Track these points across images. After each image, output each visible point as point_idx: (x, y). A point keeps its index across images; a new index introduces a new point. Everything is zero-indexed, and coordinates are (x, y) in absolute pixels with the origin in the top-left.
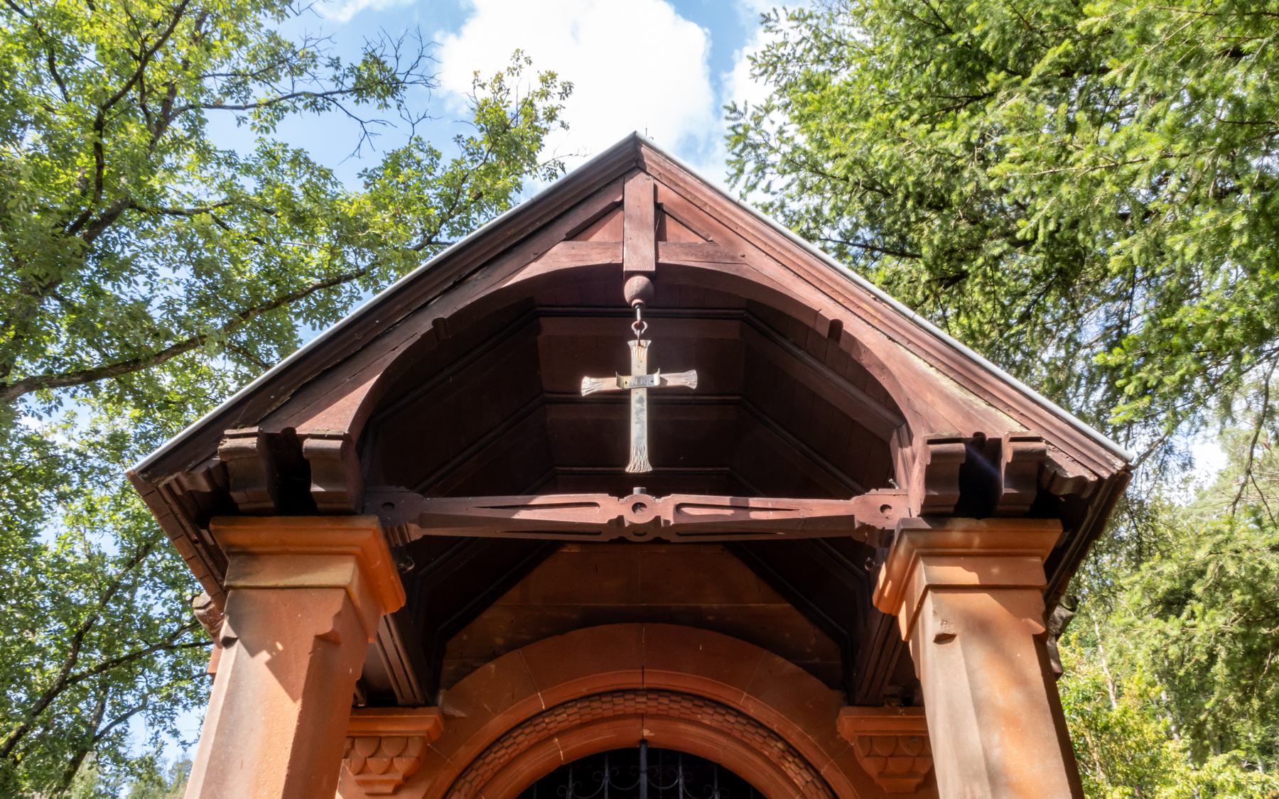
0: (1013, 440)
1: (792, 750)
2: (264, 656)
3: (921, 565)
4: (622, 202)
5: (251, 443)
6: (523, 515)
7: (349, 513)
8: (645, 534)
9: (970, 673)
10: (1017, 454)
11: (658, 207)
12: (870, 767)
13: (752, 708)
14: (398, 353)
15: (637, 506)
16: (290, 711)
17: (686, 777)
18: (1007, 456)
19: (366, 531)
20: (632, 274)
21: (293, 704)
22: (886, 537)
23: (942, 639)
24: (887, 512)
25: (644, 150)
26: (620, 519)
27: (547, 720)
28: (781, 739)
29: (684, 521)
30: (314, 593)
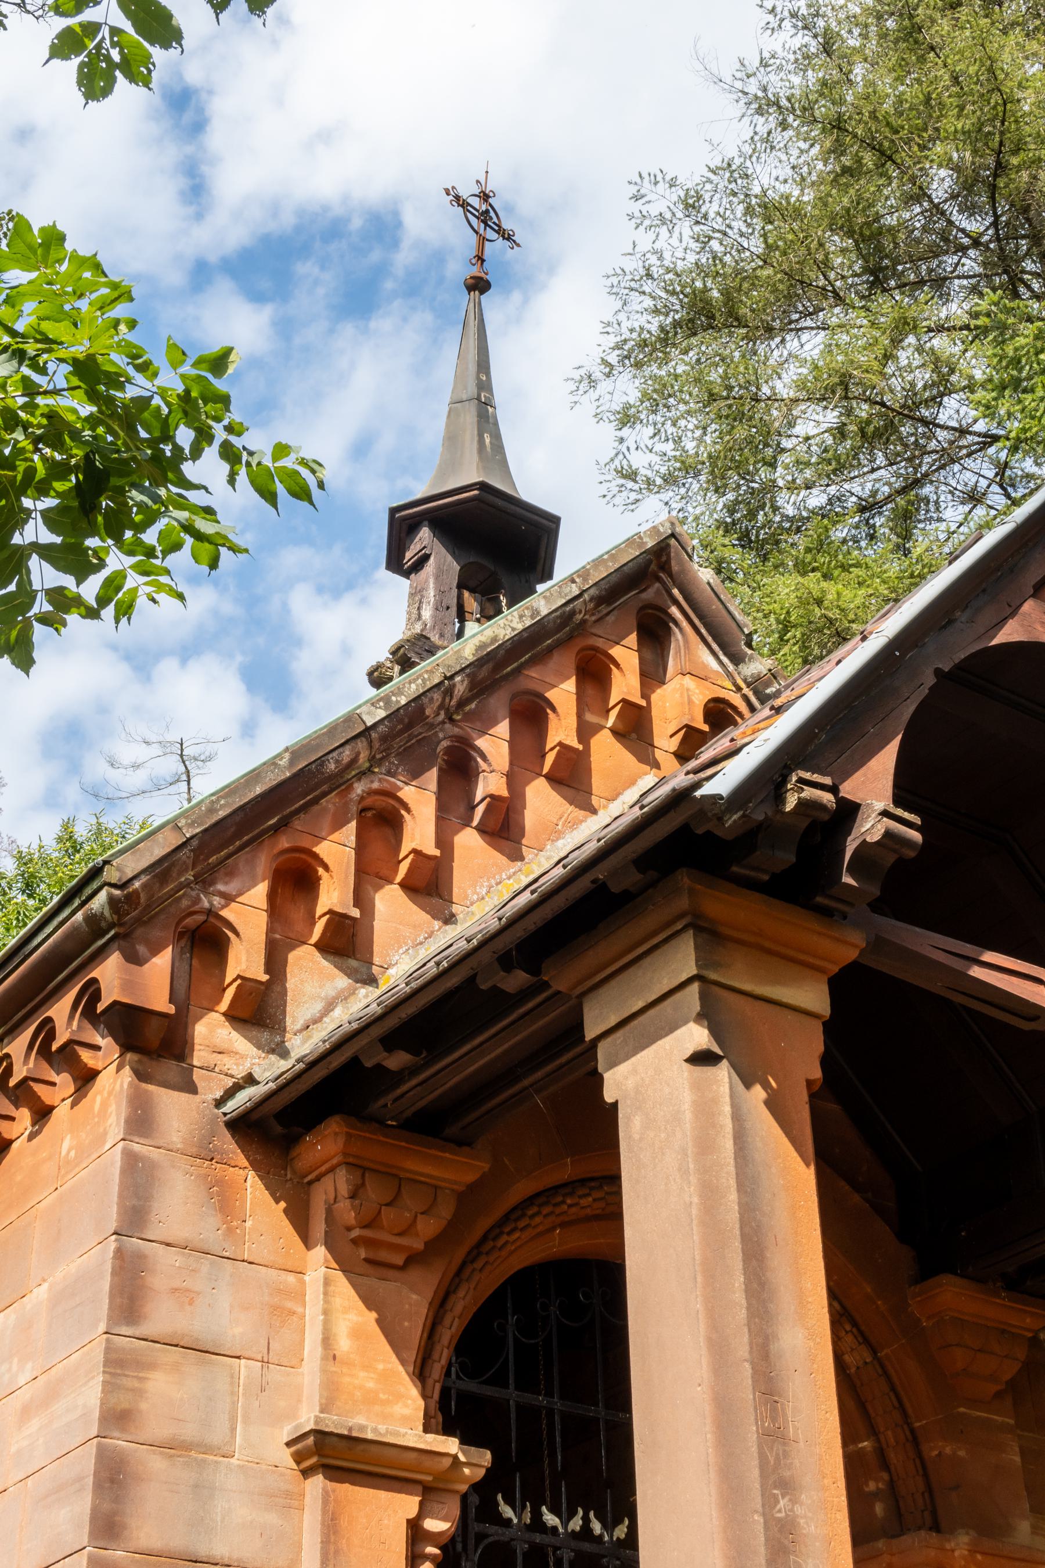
2: (758, 1093)
8: (1035, 1018)
14: (912, 709)
16: (806, 1177)
21: (807, 1170)
27: (569, 1201)
30: (790, 1016)
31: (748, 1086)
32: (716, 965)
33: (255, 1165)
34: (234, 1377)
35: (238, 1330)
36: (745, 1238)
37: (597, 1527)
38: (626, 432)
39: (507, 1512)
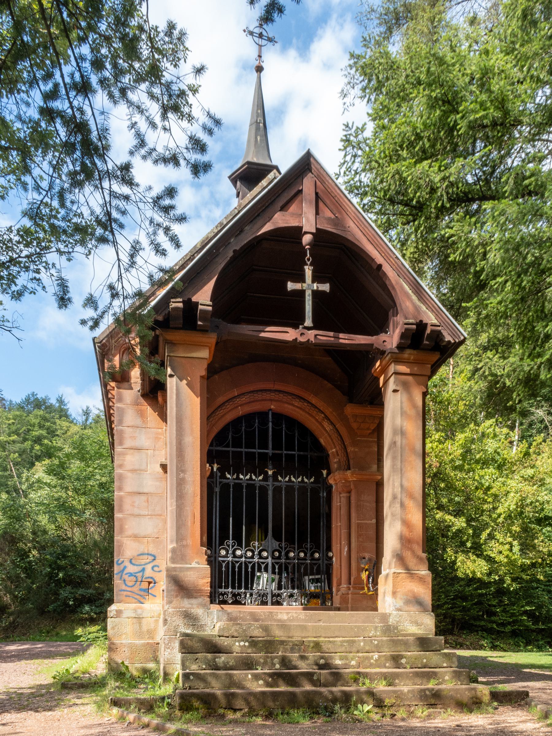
0: (432, 325)
1: (326, 417)
2: (185, 382)
3: (393, 364)
4: (302, 190)
5: (181, 305)
6: (263, 335)
7: (207, 331)
9: (401, 403)
10: (432, 331)
11: (317, 194)
12: (355, 426)
13: (314, 401)
14: (222, 266)
15: (302, 334)
16: (197, 401)
17: (286, 424)
18: (428, 331)
19: (212, 338)
20: (306, 233)
22: (383, 353)
23: (395, 391)
24: (385, 343)
25: (312, 159)
26: (296, 339)
28: (323, 413)
29: (318, 341)
30: (197, 360)
31: (181, 380)
32: (173, 352)
33: (149, 405)
34: (147, 454)
35: (147, 444)
36: (177, 418)
37: (254, 477)
38: (346, 100)
39: (228, 476)
